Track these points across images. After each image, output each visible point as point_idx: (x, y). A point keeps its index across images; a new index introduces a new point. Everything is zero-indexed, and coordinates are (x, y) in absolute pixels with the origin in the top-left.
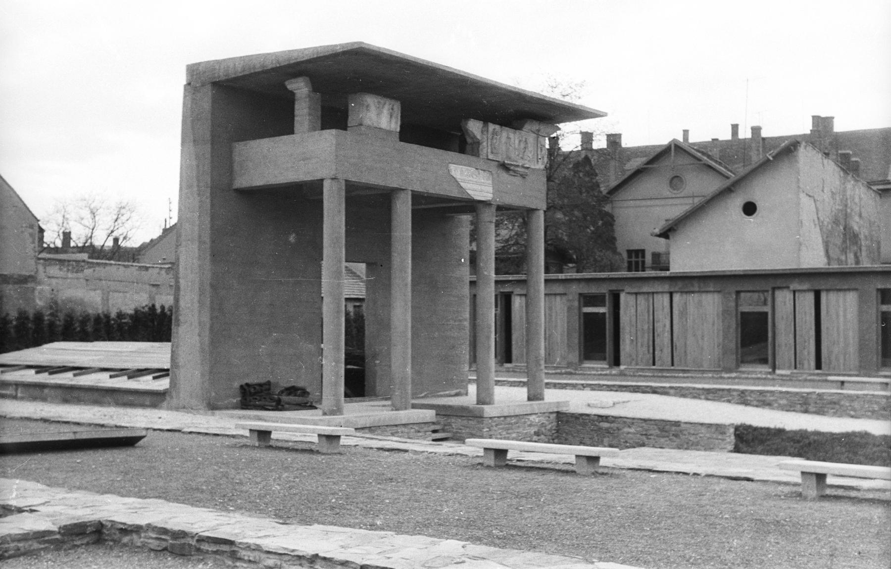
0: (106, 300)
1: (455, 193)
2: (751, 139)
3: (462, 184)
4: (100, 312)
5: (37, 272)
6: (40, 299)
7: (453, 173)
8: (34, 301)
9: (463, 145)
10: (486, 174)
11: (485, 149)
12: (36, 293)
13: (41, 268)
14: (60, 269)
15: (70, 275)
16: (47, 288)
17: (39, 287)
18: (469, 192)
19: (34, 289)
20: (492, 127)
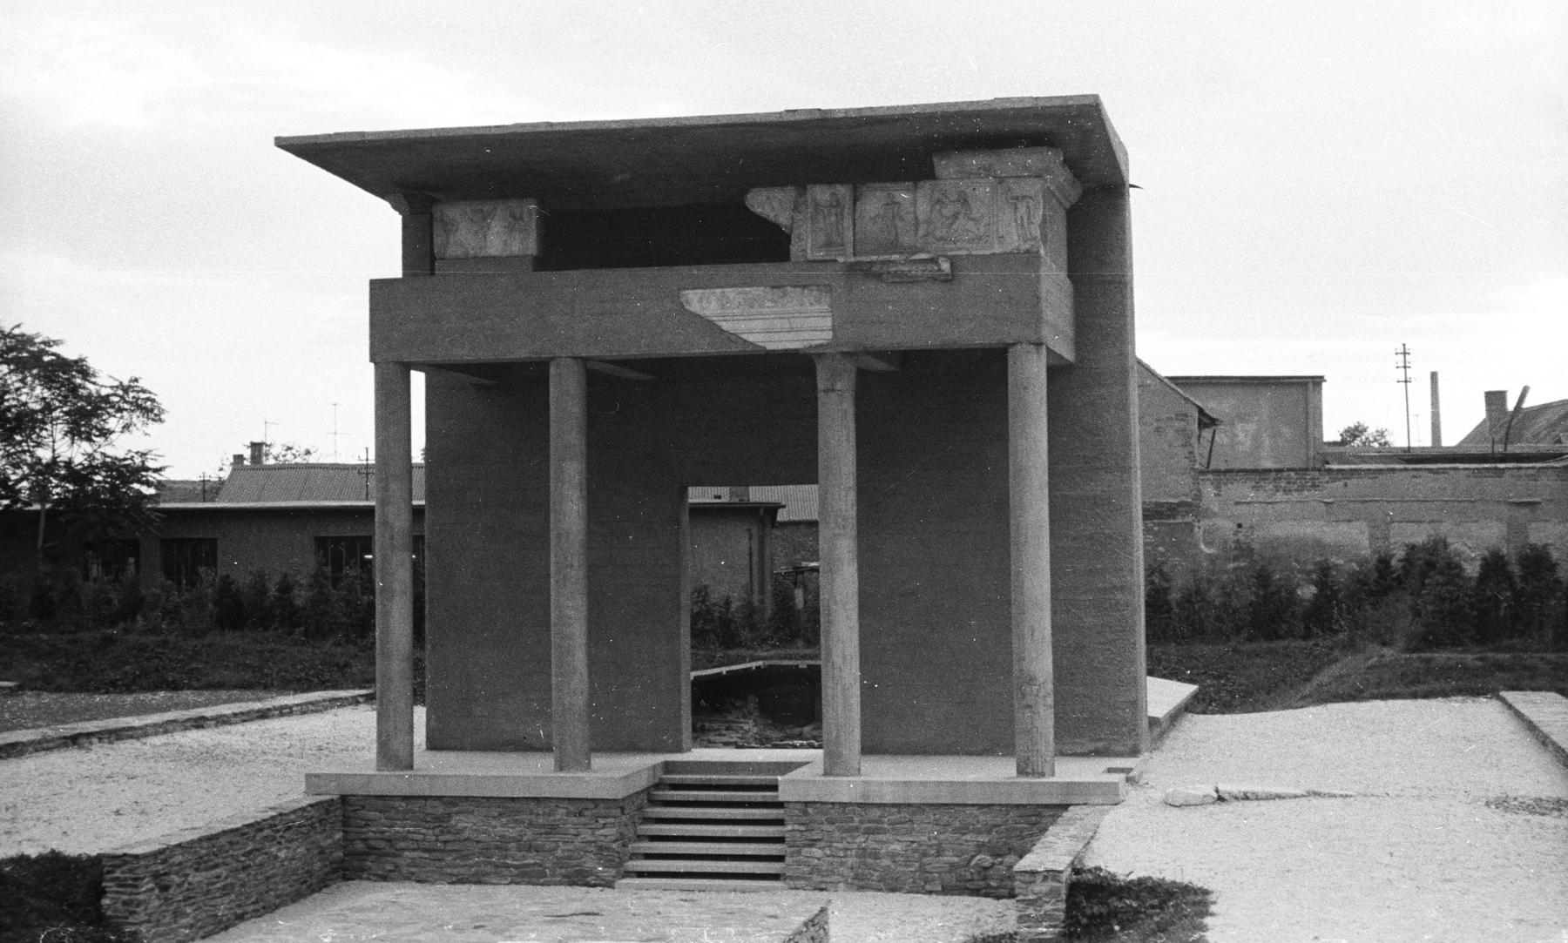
0: (1379, 528)
1: (703, 347)
2: (541, 203)
3: (725, 326)
4: (1366, 552)
5: (1199, 496)
6: (1208, 544)
7: (695, 307)
8: (1196, 546)
9: (765, 246)
10: (809, 296)
11: (806, 244)
12: (1199, 533)
13: (1209, 490)
14: (1256, 488)
15: (1280, 496)
16: (1227, 526)
17: (1205, 523)
18: (751, 338)
19: (1190, 526)
20: (821, 193)
